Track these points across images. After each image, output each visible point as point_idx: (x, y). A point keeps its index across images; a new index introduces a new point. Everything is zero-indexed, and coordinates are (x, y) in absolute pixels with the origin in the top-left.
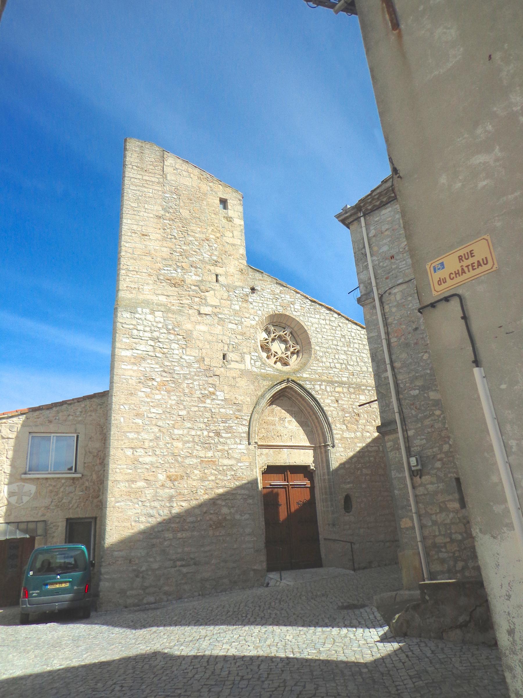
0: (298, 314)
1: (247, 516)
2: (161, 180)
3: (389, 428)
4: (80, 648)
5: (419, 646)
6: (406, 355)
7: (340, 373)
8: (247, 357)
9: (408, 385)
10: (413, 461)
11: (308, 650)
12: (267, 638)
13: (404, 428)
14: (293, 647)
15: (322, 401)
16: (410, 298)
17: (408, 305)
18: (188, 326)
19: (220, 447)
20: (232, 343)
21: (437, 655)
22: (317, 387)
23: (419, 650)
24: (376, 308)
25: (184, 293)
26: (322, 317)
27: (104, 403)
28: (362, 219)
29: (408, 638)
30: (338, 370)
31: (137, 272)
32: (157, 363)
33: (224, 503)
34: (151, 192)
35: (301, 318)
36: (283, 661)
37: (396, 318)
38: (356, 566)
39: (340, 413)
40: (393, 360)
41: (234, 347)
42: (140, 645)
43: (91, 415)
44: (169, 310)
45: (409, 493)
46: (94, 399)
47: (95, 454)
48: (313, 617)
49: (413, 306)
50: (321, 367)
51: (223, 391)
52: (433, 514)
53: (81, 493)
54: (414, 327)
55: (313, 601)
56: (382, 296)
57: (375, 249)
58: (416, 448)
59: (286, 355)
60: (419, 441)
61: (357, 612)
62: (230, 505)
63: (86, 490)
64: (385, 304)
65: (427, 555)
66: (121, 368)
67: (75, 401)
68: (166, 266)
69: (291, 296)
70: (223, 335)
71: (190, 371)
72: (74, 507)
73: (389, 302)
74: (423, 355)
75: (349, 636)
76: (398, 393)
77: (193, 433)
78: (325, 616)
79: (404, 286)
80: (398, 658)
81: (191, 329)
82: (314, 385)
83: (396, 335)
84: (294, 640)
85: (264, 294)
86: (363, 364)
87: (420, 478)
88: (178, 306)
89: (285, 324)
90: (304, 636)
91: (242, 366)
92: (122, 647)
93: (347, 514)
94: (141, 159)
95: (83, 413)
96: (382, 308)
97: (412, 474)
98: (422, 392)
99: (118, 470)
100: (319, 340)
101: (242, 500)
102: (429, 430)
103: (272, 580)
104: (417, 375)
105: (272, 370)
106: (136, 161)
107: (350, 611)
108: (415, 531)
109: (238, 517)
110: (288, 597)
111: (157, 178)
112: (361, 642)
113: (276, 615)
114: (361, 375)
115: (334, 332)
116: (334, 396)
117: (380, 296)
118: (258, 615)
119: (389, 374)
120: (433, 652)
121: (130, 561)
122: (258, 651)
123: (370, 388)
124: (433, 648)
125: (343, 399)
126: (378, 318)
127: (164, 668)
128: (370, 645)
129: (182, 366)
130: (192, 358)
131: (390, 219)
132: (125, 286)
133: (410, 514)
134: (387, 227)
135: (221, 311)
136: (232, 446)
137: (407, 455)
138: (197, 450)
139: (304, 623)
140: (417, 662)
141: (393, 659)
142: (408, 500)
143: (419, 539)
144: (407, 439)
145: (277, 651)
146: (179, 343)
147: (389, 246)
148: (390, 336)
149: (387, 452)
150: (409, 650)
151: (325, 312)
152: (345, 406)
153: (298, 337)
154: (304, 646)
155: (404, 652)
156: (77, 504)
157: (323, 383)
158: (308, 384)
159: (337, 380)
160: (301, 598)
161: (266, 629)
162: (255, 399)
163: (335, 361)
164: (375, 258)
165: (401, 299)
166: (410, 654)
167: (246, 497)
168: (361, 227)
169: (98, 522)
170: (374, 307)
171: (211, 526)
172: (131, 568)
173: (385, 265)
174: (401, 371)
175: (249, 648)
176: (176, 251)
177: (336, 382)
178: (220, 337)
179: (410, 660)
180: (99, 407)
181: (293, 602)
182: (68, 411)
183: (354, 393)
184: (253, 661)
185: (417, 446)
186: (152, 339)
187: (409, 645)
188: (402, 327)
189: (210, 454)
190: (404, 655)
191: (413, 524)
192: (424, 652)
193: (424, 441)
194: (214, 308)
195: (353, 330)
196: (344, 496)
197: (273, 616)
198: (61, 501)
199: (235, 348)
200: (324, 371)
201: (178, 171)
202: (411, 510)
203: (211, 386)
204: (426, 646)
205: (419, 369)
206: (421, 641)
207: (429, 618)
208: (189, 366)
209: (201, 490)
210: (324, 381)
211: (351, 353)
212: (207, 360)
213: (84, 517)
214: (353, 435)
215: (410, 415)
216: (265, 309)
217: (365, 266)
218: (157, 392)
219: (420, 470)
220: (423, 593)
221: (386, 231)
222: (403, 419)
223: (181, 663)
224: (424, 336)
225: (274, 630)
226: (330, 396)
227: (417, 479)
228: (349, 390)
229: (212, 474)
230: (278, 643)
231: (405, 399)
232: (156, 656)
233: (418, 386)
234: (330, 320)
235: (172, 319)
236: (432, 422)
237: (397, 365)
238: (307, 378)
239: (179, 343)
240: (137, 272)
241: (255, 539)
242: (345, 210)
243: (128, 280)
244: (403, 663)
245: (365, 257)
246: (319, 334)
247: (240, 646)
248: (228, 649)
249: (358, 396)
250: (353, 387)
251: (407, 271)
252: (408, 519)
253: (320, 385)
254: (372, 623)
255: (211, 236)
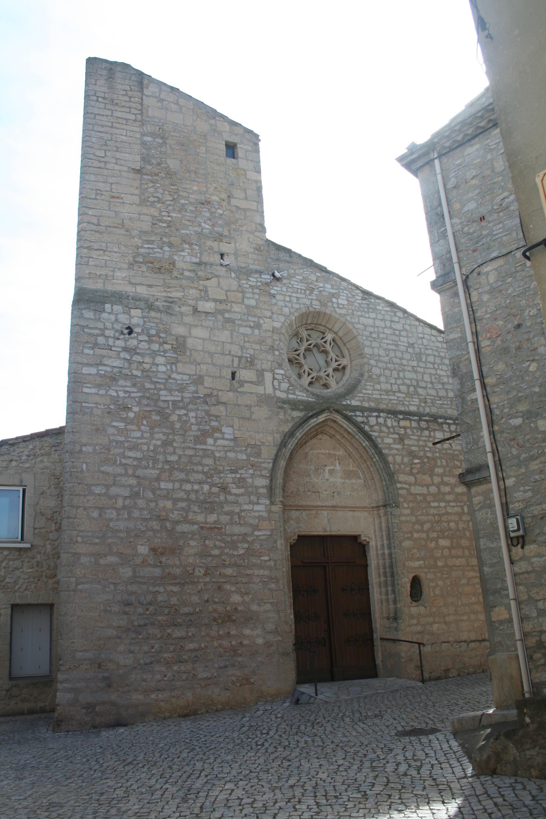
0: (343, 311)
1: (268, 607)
2: (139, 117)
3: (477, 476)
4: (24, 781)
5: (514, 789)
6: (504, 366)
7: (407, 399)
8: (268, 376)
9: (506, 410)
10: (512, 523)
11: (349, 793)
12: (290, 775)
13: (500, 475)
14: (327, 789)
15: (379, 440)
16: (509, 280)
17: (507, 290)
18: (180, 330)
19: (227, 508)
20: (244, 355)
21: (540, 802)
22: (373, 421)
23: (513, 795)
24: (458, 296)
25: (172, 281)
26: (380, 317)
27: (60, 443)
28: (437, 162)
29: (497, 778)
30: (404, 395)
31: (104, 251)
32: (134, 385)
33: (233, 589)
34: (125, 134)
35: (348, 318)
36: (311, 809)
37: (488, 310)
38: (426, 675)
39: (406, 460)
40: (484, 373)
41: (247, 361)
42: (108, 780)
43: (42, 461)
44: (151, 307)
45: (505, 570)
46: (45, 438)
47: (49, 517)
48: (360, 746)
49: (514, 291)
50: (378, 390)
51: (232, 426)
52: (540, 600)
53: (31, 570)
54: (516, 323)
55: (360, 724)
56: (467, 277)
57: (457, 206)
58: (517, 505)
59: (326, 373)
60: (521, 493)
61: (424, 739)
62: (243, 590)
63: (37, 565)
64: (471, 290)
65: (530, 658)
66: (82, 392)
67: (20, 440)
68: (148, 242)
69: (332, 285)
70: (232, 343)
71: (182, 397)
72: (22, 590)
73: (478, 286)
74: (529, 366)
75: (410, 773)
76: (491, 423)
77: (188, 487)
78: (377, 746)
79: (500, 262)
80: (481, 807)
81: (183, 334)
82: (367, 417)
83: (488, 335)
84: (329, 778)
85: (292, 282)
86: (440, 386)
87: (522, 547)
88: (165, 301)
89: (325, 326)
90: (344, 774)
91: (260, 390)
92: (83, 782)
93: (414, 604)
94: (111, 87)
95: (32, 457)
96: (468, 295)
97: (510, 542)
98: (527, 421)
99: (79, 539)
100: (376, 351)
101: (260, 584)
102: (537, 477)
103: (304, 696)
104: (520, 395)
105: (305, 395)
106: (103, 89)
107: (413, 738)
108: (513, 625)
109: (254, 608)
110: (325, 718)
111: (134, 114)
112: (427, 783)
113: (306, 743)
114: (437, 402)
115: (396, 339)
116: (398, 434)
117: (464, 277)
118: (280, 744)
119: (478, 394)
120: (534, 798)
121: (100, 666)
122: (275, 795)
123: (451, 422)
124: (534, 792)
125: (411, 437)
126: (461, 311)
127: (138, 814)
128: (441, 787)
129: (170, 391)
130: (185, 377)
131: (478, 160)
132: (87, 272)
133: (506, 601)
134: (474, 173)
135: (228, 307)
136: (246, 507)
137: (503, 516)
138: (194, 512)
139: (346, 755)
140: (510, 812)
141: (475, 808)
142: (504, 581)
143: (518, 636)
144: (504, 492)
145: (303, 795)
146: (167, 355)
147: (477, 202)
148: (480, 338)
149: (475, 511)
150: (499, 795)
151: (385, 309)
152: (414, 448)
153: (345, 344)
154: (344, 787)
155: (491, 798)
156: (25, 585)
157: (382, 414)
158: (359, 416)
159: (403, 409)
160: (343, 720)
161: (290, 763)
162: (278, 438)
163: (399, 382)
164: (456, 221)
165: (496, 282)
166: (500, 800)
167: (267, 580)
168: (435, 175)
169: (55, 610)
170: (456, 294)
171: (215, 620)
172: (101, 675)
173: (471, 231)
174: (496, 390)
175: (264, 789)
176: (162, 221)
177: (401, 413)
178: (228, 346)
179: (499, 810)
180: (54, 448)
181: (332, 725)
182: (9, 454)
183: (427, 429)
184: (268, 808)
185: (519, 501)
186: (125, 349)
187: (499, 788)
188: (497, 323)
189: (212, 518)
190: (490, 802)
191: (510, 615)
192: (521, 798)
193: (530, 494)
194: (218, 303)
195: (425, 336)
196: (411, 578)
197: (302, 744)
198: (4, 580)
199: (251, 362)
200: (383, 397)
201: (164, 103)
202: (507, 596)
203: (214, 419)
204: (524, 788)
205: (522, 385)
206: (516, 782)
207: (529, 749)
208: (182, 389)
209: (201, 569)
210: (383, 411)
211: (422, 370)
212: (208, 381)
213: (36, 603)
214: (424, 491)
215: (510, 455)
216: (294, 305)
217: (442, 232)
218: (134, 427)
219: (523, 537)
220: (521, 714)
221: (472, 179)
222: (498, 462)
223: (163, 808)
224: (531, 336)
225: (301, 765)
226: (393, 434)
227: (517, 551)
228: (419, 424)
229: (215, 547)
230: (305, 783)
231: (502, 432)
232: (128, 796)
233: (521, 412)
234: (392, 321)
235: (156, 321)
236: (541, 465)
237: (489, 381)
238: (357, 406)
239: (167, 355)
240: (104, 251)
241: (281, 639)
242: (413, 149)
243: (91, 263)
244: (490, 814)
245: (441, 219)
246: (375, 341)
247: (249, 786)
248: (233, 790)
249: (432, 434)
250: (425, 421)
251: (504, 238)
252: (503, 608)
253: (377, 417)
254: (445, 755)
255: (214, 198)
